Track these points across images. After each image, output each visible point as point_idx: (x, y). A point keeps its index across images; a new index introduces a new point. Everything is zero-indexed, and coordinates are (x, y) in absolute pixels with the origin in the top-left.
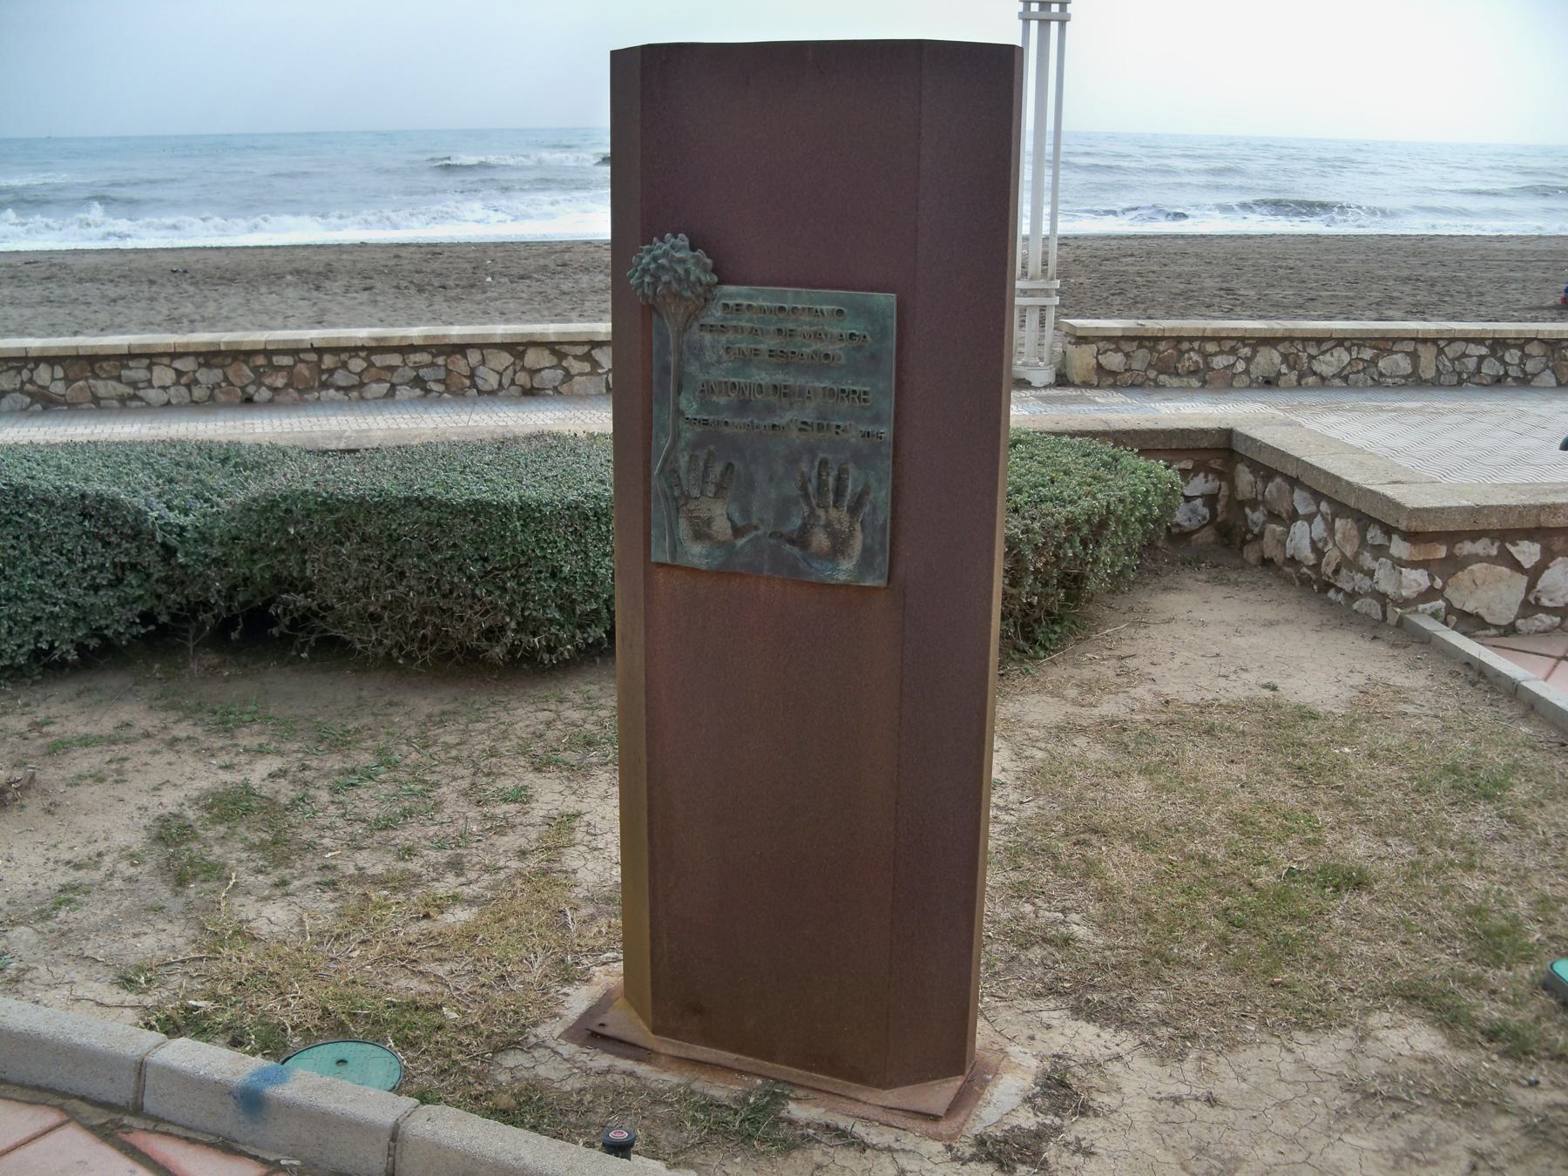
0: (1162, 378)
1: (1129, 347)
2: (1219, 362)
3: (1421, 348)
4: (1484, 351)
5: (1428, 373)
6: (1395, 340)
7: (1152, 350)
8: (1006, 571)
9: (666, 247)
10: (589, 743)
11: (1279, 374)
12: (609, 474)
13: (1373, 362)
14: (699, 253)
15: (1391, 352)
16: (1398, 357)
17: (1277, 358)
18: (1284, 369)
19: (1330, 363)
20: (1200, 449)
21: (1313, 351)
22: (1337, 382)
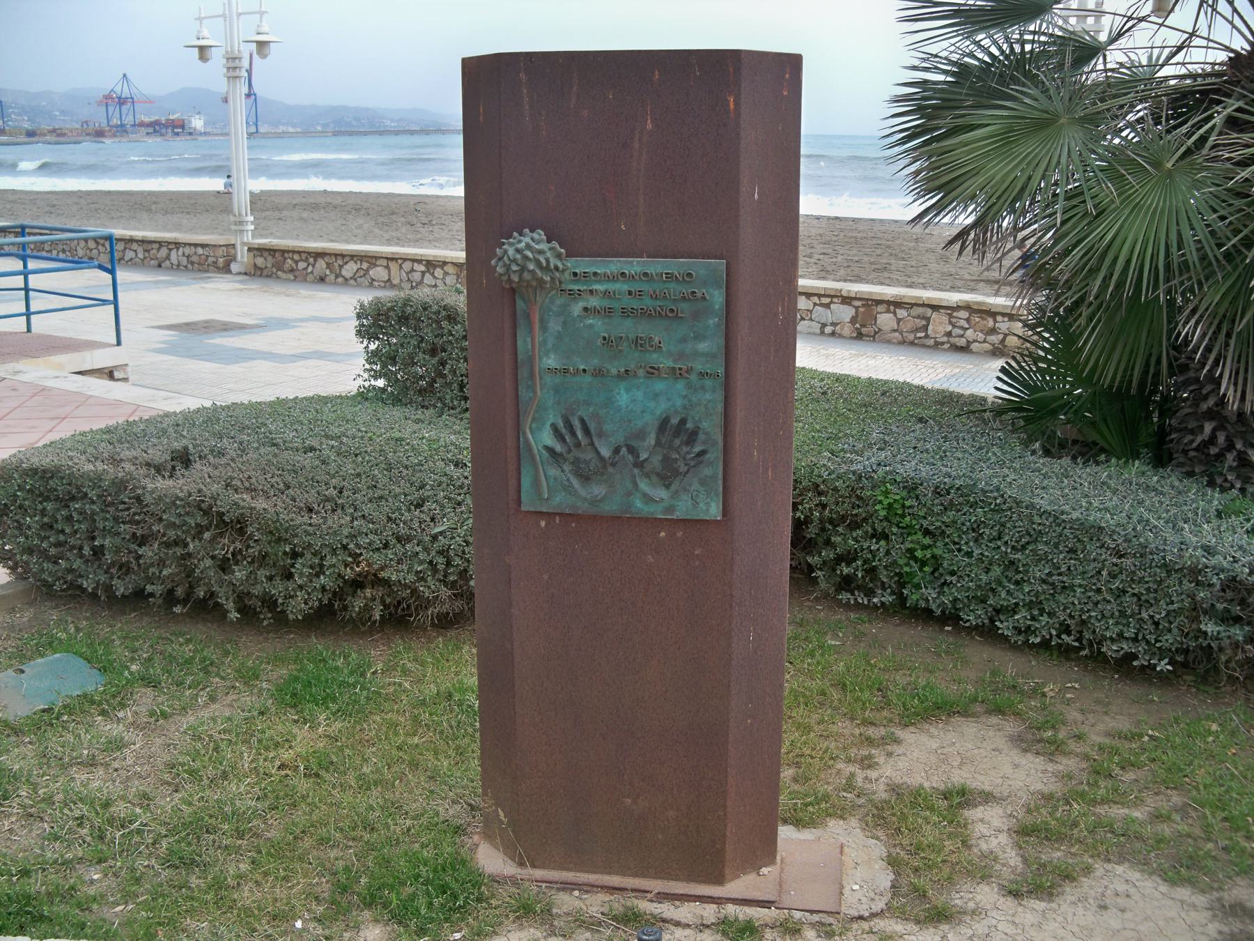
0: (279, 273)
1: (266, 254)
2: (302, 265)
3: (390, 263)
4: (423, 268)
5: (395, 281)
6: (377, 258)
7: (273, 256)
8: (1047, 453)
9: (527, 239)
10: (256, 882)
11: (326, 275)
12: (798, 345)
13: (367, 271)
14: (555, 244)
15: (375, 265)
16: (379, 269)
17: (324, 266)
18: (328, 272)
19: (350, 269)
20: (727, 347)
21: (340, 262)
22: (352, 282)
